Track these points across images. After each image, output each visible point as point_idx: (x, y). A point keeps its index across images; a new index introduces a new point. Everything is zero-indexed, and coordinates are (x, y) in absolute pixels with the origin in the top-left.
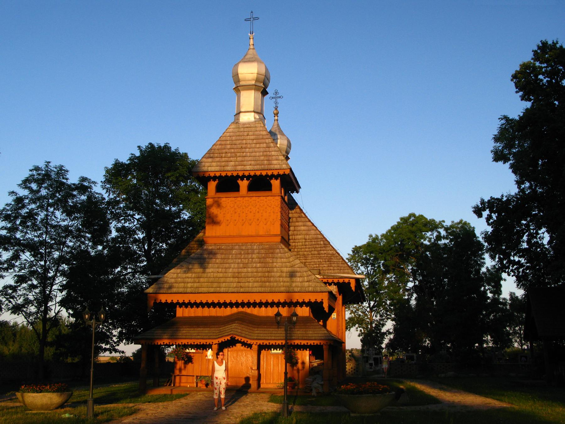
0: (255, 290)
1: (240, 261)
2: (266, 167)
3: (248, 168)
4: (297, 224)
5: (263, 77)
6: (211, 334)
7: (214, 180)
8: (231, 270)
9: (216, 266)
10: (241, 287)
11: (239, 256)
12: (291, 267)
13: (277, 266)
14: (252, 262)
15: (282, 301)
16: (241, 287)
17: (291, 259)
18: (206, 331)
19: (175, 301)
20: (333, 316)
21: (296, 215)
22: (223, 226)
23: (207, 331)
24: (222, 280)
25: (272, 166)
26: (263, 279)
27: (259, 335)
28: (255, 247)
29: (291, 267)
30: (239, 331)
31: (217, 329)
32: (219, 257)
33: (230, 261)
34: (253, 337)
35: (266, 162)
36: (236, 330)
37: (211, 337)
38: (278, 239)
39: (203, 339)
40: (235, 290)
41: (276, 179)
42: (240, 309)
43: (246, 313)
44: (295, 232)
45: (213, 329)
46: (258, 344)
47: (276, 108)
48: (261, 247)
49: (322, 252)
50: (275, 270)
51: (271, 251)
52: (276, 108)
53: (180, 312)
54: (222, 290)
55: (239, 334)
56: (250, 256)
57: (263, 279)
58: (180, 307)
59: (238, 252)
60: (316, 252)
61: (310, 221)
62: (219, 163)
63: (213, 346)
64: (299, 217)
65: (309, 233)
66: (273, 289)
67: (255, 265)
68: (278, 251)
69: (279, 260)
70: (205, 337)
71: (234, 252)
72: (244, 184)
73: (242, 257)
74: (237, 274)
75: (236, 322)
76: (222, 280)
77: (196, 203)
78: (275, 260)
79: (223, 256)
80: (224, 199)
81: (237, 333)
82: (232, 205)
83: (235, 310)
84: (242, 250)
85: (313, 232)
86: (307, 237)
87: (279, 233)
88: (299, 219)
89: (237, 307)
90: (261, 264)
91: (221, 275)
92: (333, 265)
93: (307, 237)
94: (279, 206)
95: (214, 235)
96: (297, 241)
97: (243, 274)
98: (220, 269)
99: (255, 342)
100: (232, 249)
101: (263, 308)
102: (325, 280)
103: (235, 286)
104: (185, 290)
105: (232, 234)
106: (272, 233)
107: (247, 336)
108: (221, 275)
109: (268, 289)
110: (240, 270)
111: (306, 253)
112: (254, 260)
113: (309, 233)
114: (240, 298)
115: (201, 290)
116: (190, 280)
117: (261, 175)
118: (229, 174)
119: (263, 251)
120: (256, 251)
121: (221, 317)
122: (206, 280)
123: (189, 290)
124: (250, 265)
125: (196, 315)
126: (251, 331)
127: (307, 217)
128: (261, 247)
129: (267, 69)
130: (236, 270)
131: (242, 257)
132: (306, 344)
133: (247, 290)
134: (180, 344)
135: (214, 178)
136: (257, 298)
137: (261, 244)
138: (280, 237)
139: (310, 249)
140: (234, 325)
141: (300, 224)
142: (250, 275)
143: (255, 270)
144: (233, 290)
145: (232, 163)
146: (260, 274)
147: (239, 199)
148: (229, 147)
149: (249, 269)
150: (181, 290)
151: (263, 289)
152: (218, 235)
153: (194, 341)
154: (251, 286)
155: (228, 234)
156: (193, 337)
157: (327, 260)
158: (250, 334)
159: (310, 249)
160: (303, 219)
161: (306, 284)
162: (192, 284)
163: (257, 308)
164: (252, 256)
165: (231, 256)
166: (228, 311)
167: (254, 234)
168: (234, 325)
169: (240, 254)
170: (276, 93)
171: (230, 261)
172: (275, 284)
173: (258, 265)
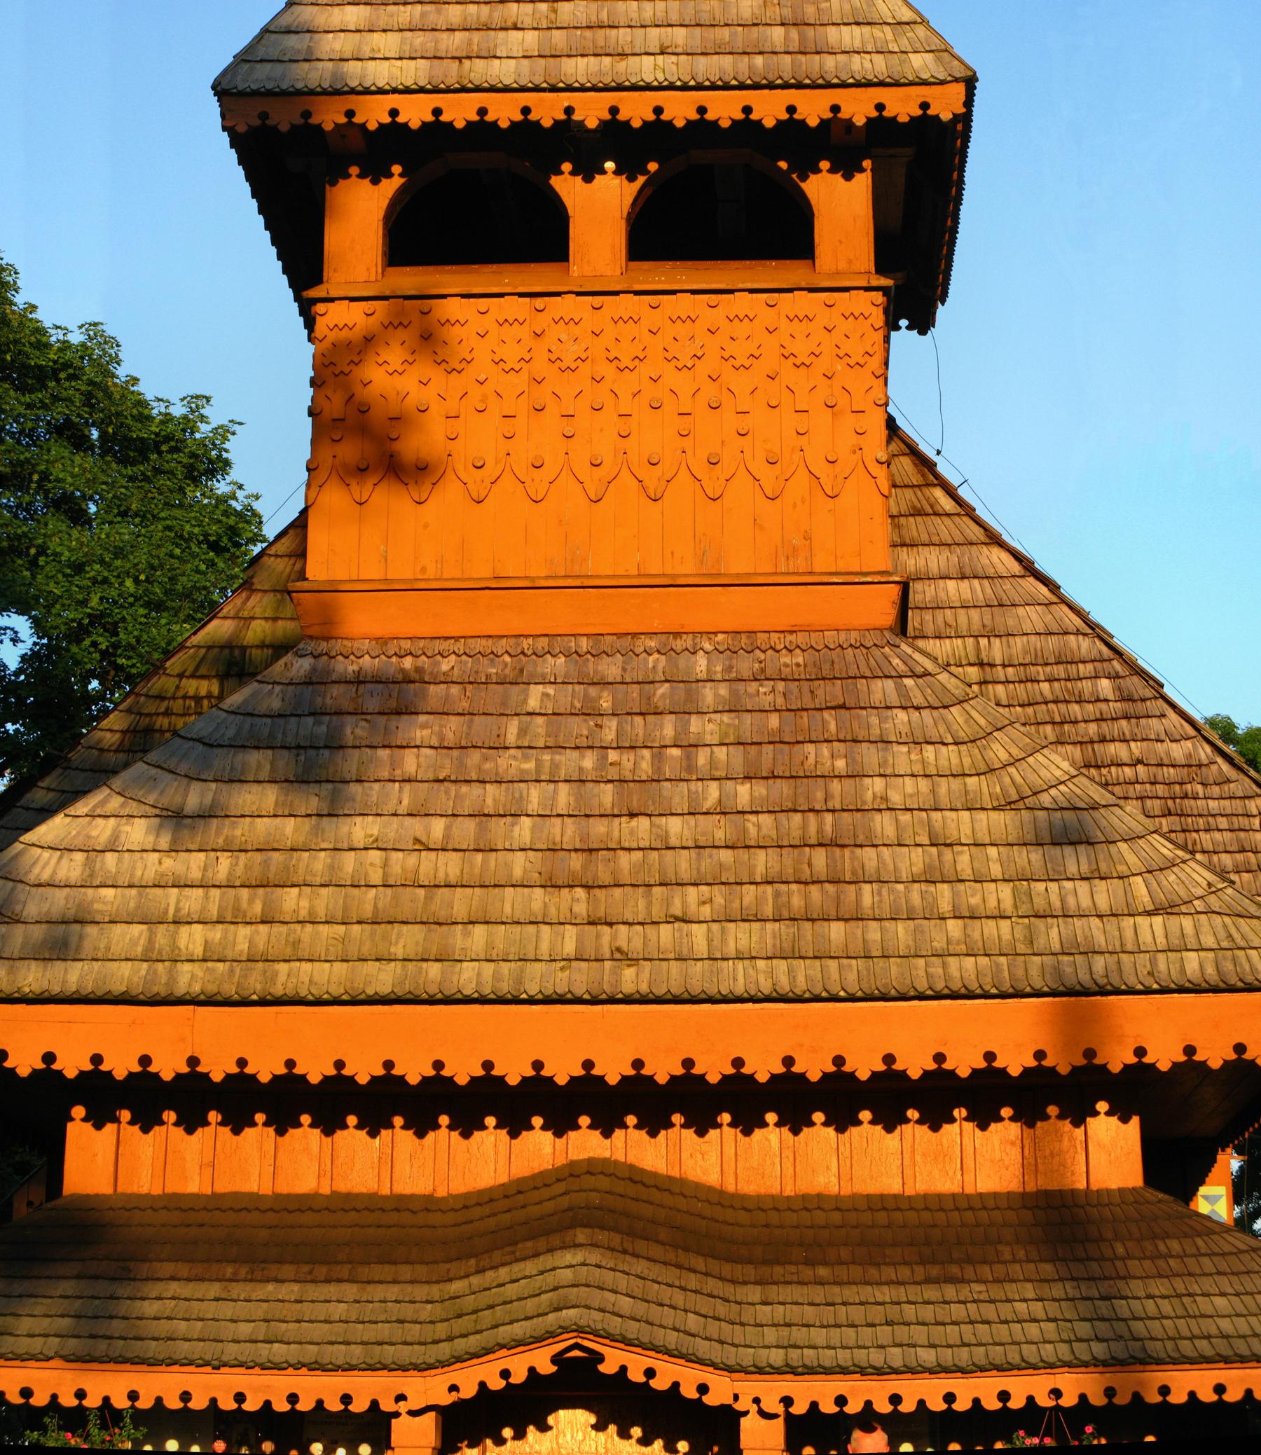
0: (739, 978)
1: (588, 761)
2: (786, 66)
6: (383, 1331)
7: (376, 174)
8: (524, 830)
9: (406, 797)
10: (622, 956)
11: (579, 727)
13: (896, 798)
14: (689, 774)
15: (1015, 1062)
16: (622, 956)
17: (999, 751)
18: (335, 1302)
19: (71, 1064)
22: (446, 500)
23: (339, 1310)
24: (461, 903)
25: (830, 62)
26: (796, 897)
27: (799, 1335)
28: (701, 662)
30: (625, 1304)
31: (421, 1292)
32: (420, 735)
33: (509, 763)
34: (747, 1356)
35: (778, 33)
36: (597, 1297)
37: (389, 1353)
39: (862, 1371)
40: (580, 979)
41: (848, 169)
42: (586, 1142)
43: (635, 1176)
45: (393, 1291)
46: (800, 1408)
48: (746, 665)
51: (834, 692)
53: (95, 1159)
54: (467, 978)
55: (632, 1330)
56: (668, 728)
57: (796, 897)
58: (98, 1119)
59: (567, 697)
61: (994, 539)
62: (419, 39)
63: (399, 1427)
64: (917, 513)
65: (1010, 619)
66: (893, 974)
67: (713, 790)
68: (883, 690)
70: (338, 1354)
71: (534, 698)
72: (599, 205)
73: (609, 733)
74: (576, 861)
75: (581, 1235)
76: (461, 903)
77: (78, 568)
78: (870, 756)
79: (452, 728)
80: (453, 308)
81: (615, 1325)
82: (512, 354)
83: (540, 1148)
84: (603, 684)
85: (1032, 617)
86: (997, 651)
89: (560, 1125)
90: (761, 789)
91: (450, 865)
93: (997, 651)
95: (372, 572)
97: (624, 859)
98: (438, 827)
99: (771, 1392)
100: (520, 680)
101: (771, 1136)
103: (570, 948)
104: (160, 978)
106: (822, 563)
107: (703, 1348)
108: (450, 865)
109: (851, 975)
110: (599, 828)
112: (702, 757)
113: (1010, 619)
114: (611, 1045)
115: (285, 978)
116: (192, 900)
117: (747, 127)
118: (504, 112)
119: (764, 694)
120: (708, 695)
121: (428, 1204)
122: (325, 900)
123: (189, 978)
124: (677, 795)
125: (224, 1186)
126: (721, 1309)
127: (967, 510)
128: (746, 665)
130: (568, 832)
131: (609, 733)
132: (937, 1405)
133: (674, 977)
134: (121, 1402)
135: (381, 148)
136: (761, 1045)
137: (744, 640)
140: (569, 1257)
142: (684, 864)
143: (720, 830)
144: (559, 981)
146: (762, 862)
147: (566, 306)
149: (675, 827)
150: (123, 976)
151: (804, 975)
152: (402, 571)
153: (839, 1386)
154: (701, 948)
155: (481, 571)
156: (232, 1351)
157: (1155, 806)
158: (713, 1328)
160: (944, 529)
161: (1153, 929)
162: (217, 933)
163: (724, 1135)
164: (683, 730)
165: (512, 730)
166: (488, 1159)
167: (686, 567)
168: (568, 1264)
169: (590, 712)
171: (509, 763)
172: (902, 931)
173: (744, 793)
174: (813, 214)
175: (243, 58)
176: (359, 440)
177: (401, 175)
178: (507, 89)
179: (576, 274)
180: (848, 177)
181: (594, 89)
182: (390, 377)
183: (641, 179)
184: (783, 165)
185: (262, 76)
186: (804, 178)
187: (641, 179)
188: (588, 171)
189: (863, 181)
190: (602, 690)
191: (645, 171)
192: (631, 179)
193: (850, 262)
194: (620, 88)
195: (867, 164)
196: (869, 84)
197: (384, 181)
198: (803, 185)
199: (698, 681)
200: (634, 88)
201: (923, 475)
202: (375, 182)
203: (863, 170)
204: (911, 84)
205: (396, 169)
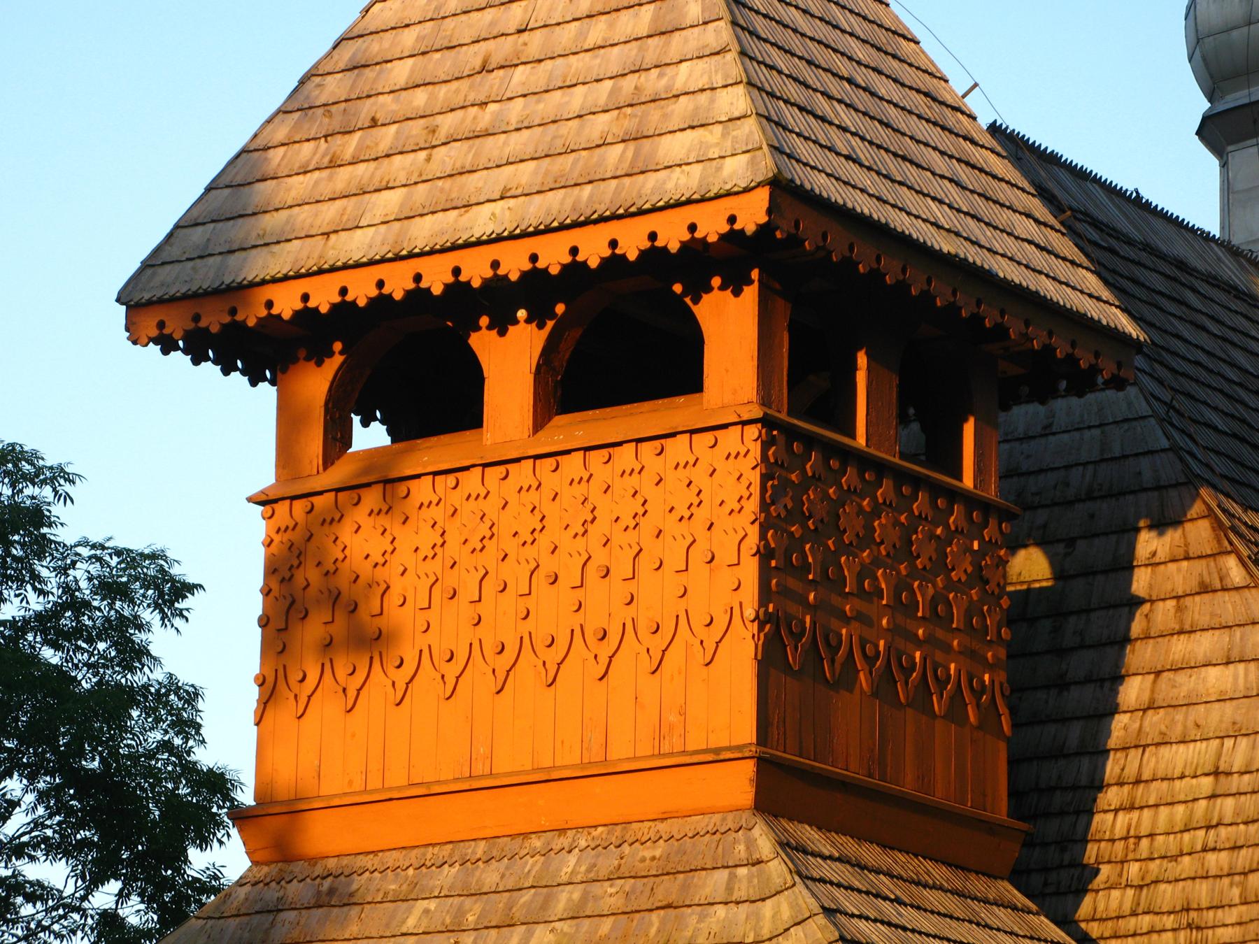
3: (482, 222)
4: (1179, 647)
7: (319, 355)
21: (1180, 576)
38: (738, 782)
41: (736, 285)
44: (1154, 720)
51: (668, 889)
64: (1205, 589)
72: (509, 360)
87: (746, 732)
88: (1199, 609)
94: (752, 506)
96: (1154, 792)
105: (425, 773)
111: (1202, 892)
119: (610, 896)
128: (608, 862)
137: (620, 829)
138: (749, 767)
141: (1204, 645)
145: (389, 202)
148: (401, 72)
155: (397, 778)
167: (570, 757)
174: (483, 379)
175: (151, 264)
176: (311, 608)
177: (341, 353)
178: (358, 265)
179: (489, 443)
180: (737, 293)
181: (512, 237)
182: (361, 540)
183: (550, 324)
184: (678, 288)
185: (174, 280)
186: (696, 301)
187: (550, 324)
188: (502, 324)
189: (751, 294)
190: (476, 902)
191: (553, 315)
192: (541, 326)
193: (735, 392)
194: (455, 247)
195: (755, 274)
196: (678, 204)
197: (327, 361)
198: (695, 309)
199: (559, 885)
200: (467, 245)
201: (1219, 541)
202: (319, 363)
203: (751, 282)
204: (718, 197)
205: (338, 346)
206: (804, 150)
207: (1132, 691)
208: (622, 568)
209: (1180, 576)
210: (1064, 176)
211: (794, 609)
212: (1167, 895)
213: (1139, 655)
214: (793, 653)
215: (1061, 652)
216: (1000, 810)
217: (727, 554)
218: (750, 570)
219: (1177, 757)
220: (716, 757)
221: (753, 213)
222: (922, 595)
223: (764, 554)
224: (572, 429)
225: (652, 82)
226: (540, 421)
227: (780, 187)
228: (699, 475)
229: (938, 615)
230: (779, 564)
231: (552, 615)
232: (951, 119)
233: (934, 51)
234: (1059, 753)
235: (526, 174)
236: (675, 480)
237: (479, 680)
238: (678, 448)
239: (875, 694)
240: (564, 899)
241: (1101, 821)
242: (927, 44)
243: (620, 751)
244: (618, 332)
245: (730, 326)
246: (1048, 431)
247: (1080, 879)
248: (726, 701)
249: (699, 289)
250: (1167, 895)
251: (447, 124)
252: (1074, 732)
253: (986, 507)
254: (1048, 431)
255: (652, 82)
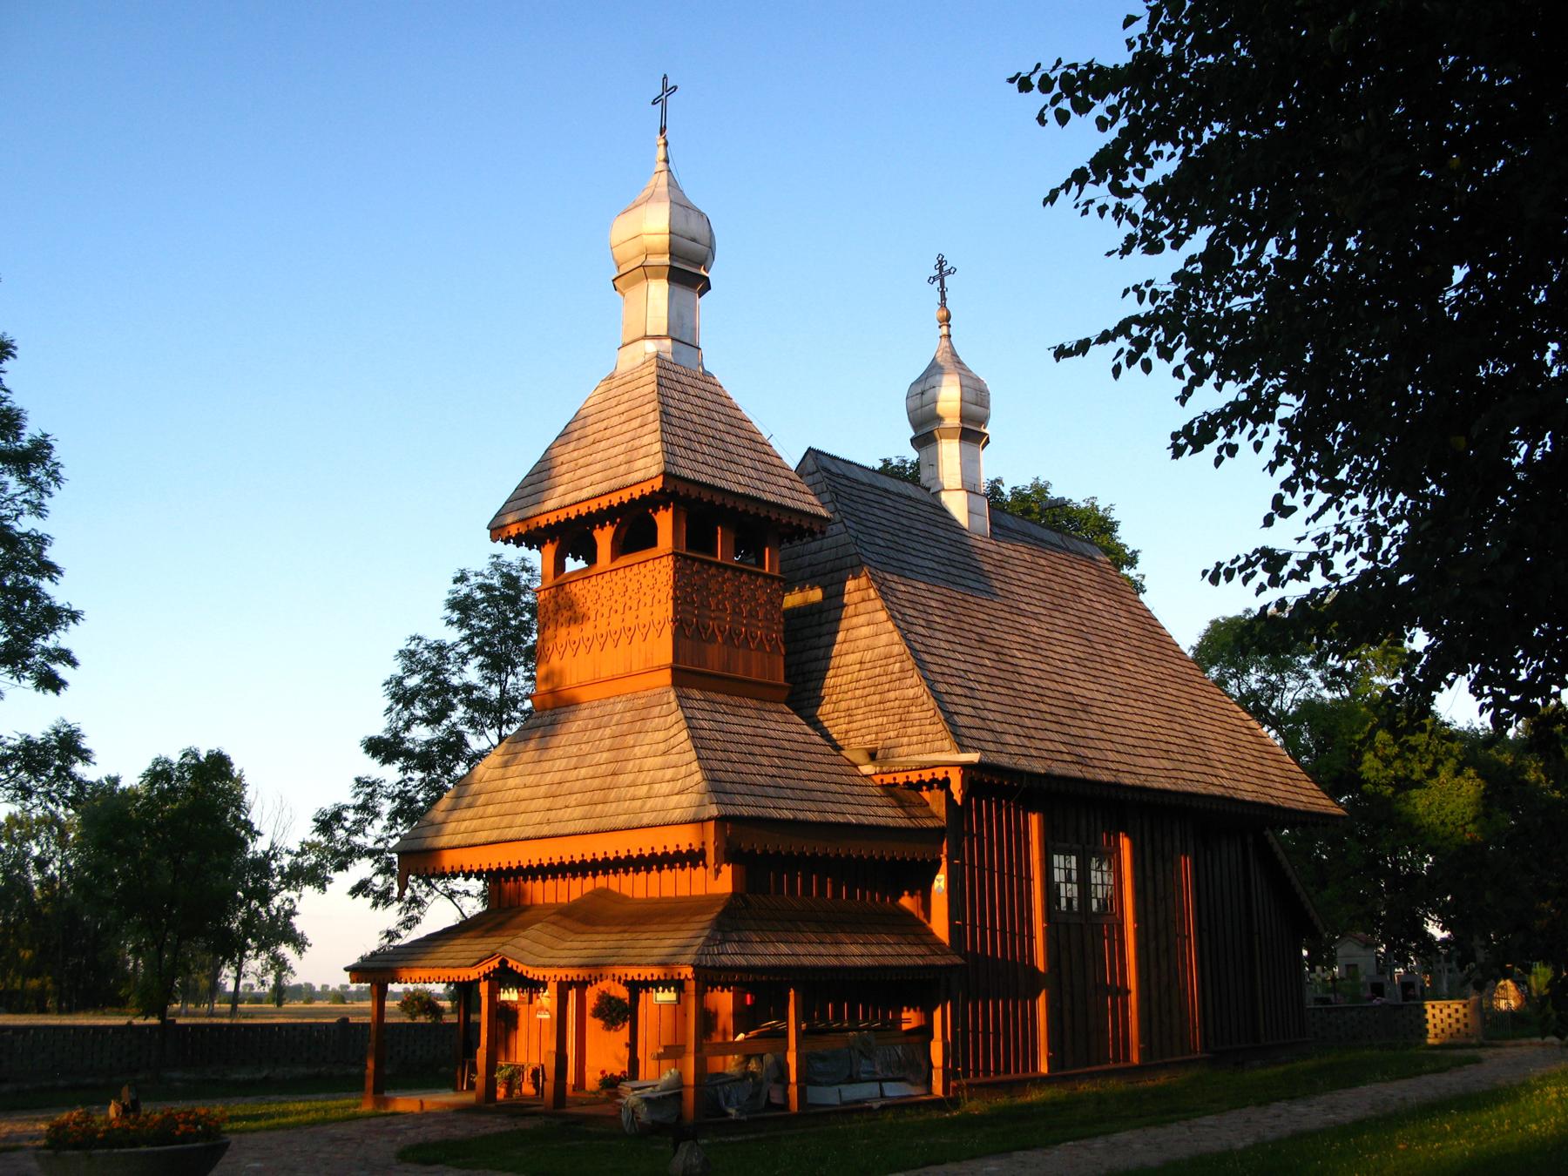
3: (584, 494)
4: (855, 621)
5: (667, 237)
8: (548, 778)
10: (549, 822)
12: (664, 753)
17: (673, 731)
20: (936, 884)
21: (856, 597)
29: (664, 753)
38: (666, 677)
41: (666, 508)
42: (601, 881)
43: (604, 893)
47: (943, 305)
49: (892, 695)
50: (630, 765)
52: (943, 305)
60: (877, 698)
69: (649, 738)
72: (604, 538)
86: (868, 656)
87: (669, 660)
88: (862, 607)
92: (910, 731)
102: (888, 779)
111: (853, 703)
129: (680, 204)
139: (866, 691)
146: (596, 783)
159: (866, 691)
167: (621, 671)
170: (940, 262)
188: (602, 527)
206: (680, 461)
207: (840, 637)
208: (635, 607)
209: (856, 597)
210: (841, 464)
211: (689, 617)
212: (843, 705)
213: (844, 624)
214: (687, 630)
215: (820, 625)
216: (782, 681)
217: (663, 596)
218: (671, 603)
219: (850, 658)
220: (659, 669)
221: (658, 484)
222: (745, 609)
223: (675, 599)
224: (623, 561)
225: (637, 443)
226: (613, 559)
227: (666, 475)
228: (641, 577)
229: (752, 615)
230: (681, 600)
231: (616, 623)
232: (759, 447)
233: (758, 425)
234: (817, 659)
235: (598, 477)
236: (649, 576)
237: (596, 647)
238: (650, 564)
239: (725, 643)
240: (616, 717)
241: (829, 682)
242: (755, 423)
243: (635, 668)
244: (631, 525)
245: (664, 521)
246: (821, 550)
247: (819, 701)
248: (662, 649)
249: (656, 511)
250: (843, 705)
251: (581, 462)
252: (821, 652)
253: (773, 578)
254: (821, 550)
255: (637, 443)
